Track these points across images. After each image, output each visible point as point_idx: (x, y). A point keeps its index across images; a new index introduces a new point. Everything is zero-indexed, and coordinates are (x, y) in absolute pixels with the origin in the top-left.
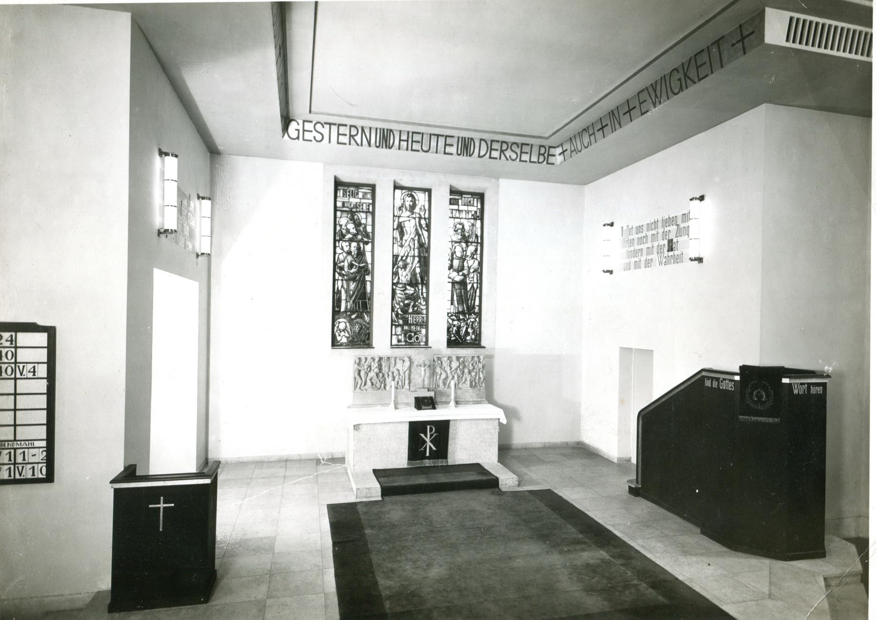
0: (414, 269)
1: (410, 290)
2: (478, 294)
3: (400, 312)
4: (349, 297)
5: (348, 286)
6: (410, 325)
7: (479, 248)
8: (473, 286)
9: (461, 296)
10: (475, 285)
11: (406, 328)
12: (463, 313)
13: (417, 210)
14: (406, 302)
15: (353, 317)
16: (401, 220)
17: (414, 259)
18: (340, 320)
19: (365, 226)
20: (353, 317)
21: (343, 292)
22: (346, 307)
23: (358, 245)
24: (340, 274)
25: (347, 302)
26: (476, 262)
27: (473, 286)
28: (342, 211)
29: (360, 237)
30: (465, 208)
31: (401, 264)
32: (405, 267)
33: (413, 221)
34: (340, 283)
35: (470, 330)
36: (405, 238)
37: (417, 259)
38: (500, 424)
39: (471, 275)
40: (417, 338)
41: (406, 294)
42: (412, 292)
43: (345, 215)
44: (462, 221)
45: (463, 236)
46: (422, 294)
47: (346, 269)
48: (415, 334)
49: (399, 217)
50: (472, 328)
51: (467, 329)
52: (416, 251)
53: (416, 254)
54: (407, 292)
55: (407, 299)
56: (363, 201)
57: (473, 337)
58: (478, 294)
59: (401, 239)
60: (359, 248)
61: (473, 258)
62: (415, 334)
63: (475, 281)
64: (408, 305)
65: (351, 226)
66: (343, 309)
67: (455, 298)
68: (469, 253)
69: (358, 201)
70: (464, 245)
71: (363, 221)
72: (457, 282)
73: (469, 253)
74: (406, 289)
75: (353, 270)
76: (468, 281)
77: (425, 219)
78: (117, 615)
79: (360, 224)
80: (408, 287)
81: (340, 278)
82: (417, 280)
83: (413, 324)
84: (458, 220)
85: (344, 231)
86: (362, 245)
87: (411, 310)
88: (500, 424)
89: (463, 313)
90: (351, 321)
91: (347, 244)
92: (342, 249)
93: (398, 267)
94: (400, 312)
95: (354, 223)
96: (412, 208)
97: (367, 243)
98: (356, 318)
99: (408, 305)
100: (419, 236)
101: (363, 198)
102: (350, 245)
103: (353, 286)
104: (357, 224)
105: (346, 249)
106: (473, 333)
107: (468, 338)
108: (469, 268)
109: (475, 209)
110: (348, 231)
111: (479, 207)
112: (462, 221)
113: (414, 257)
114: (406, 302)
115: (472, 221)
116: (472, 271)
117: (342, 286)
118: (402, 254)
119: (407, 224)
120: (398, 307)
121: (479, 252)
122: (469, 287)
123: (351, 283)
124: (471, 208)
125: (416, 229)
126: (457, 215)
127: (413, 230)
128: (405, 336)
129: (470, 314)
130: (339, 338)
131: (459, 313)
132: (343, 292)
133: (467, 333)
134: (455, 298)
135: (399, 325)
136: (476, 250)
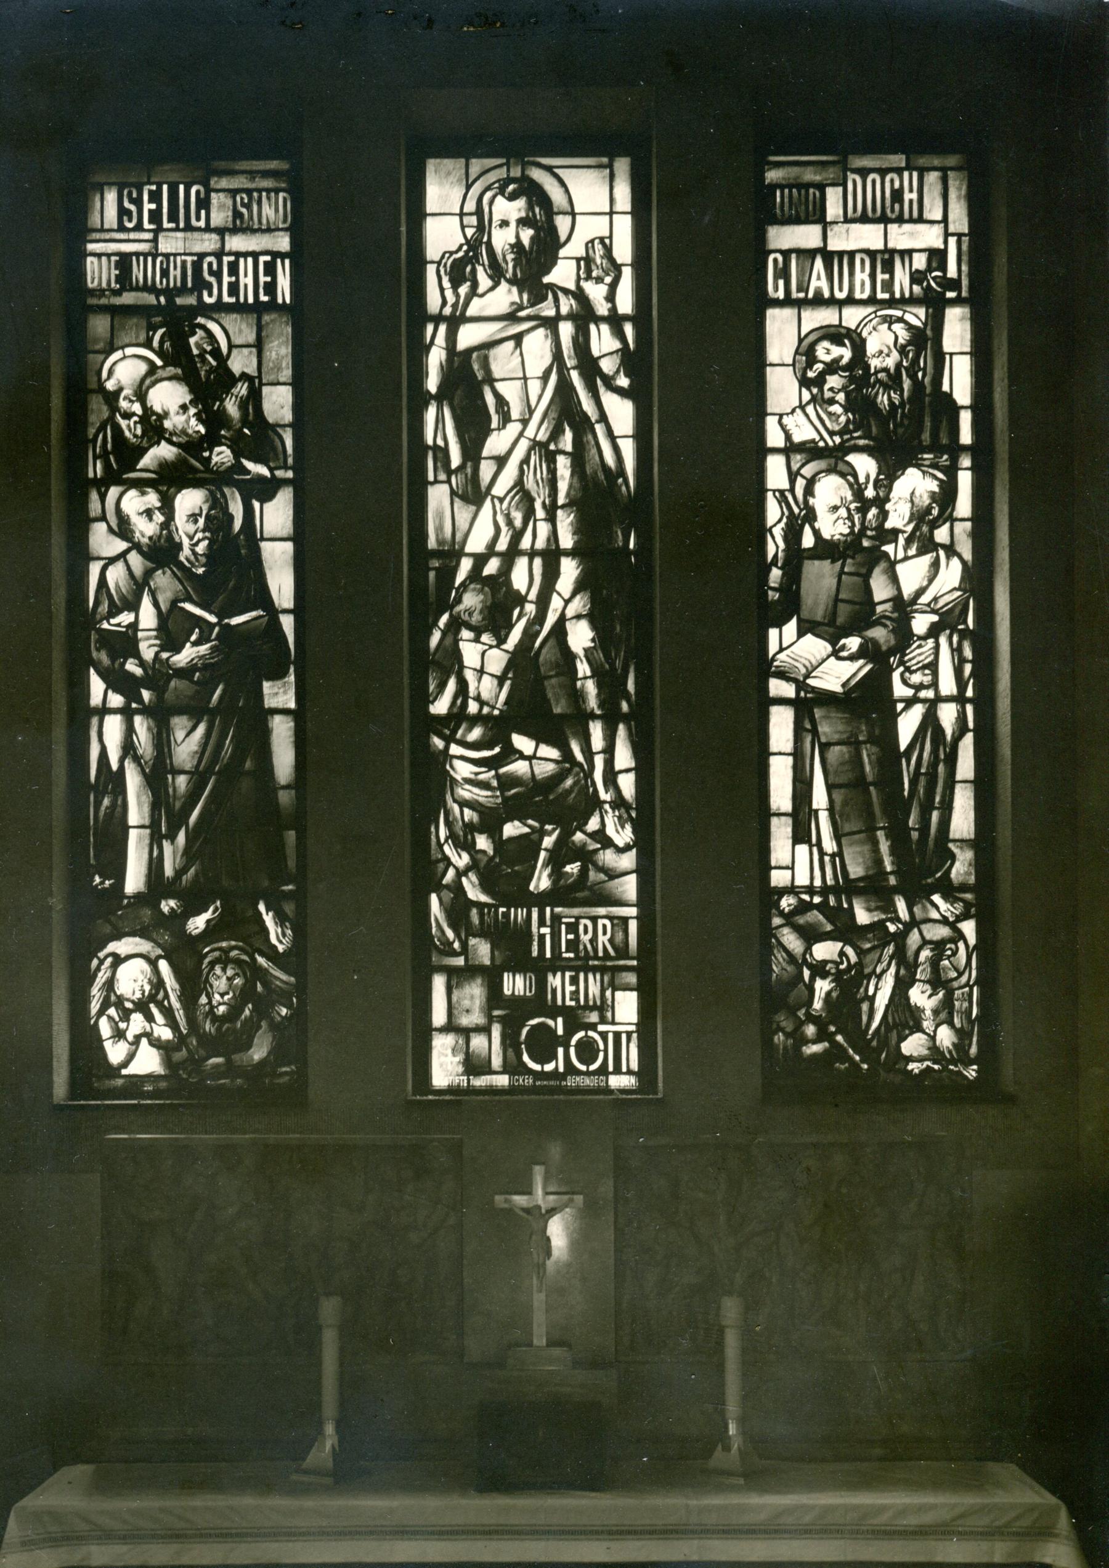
0: (560, 630)
1: (534, 757)
2: (966, 766)
3: (474, 892)
4: (165, 816)
5: (162, 740)
6: (540, 969)
7: (965, 480)
8: (930, 720)
9: (859, 783)
10: (948, 714)
11: (515, 985)
12: (874, 888)
13: (563, 274)
14: (511, 829)
15: (198, 923)
16: (469, 336)
17: (551, 574)
18: (122, 946)
19: (255, 386)
20: (198, 923)
21: (133, 780)
22: (155, 866)
23: (218, 504)
24: (117, 680)
25: (156, 838)
26: (951, 574)
27: (930, 720)
28: (115, 311)
29: (222, 455)
30: (869, 236)
31: (471, 600)
32: (496, 620)
33: (537, 345)
34: (113, 726)
35: (919, 996)
36: (496, 443)
37: (569, 570)
38: (155, 1022)
39: (920, 653)
40: (587, 1051)
41: (507, 782)
42: (543, 770)
43: (134, 329)
44: (852, 317)
45: (859, 403)
46: (611, 777)
47: (148, 652)
48: (574, 1022)
49: (456, 321)
50: (937, 982)
51: (902, 986)
52: (565, 522)
53: (567, 541)
54: (520, 767)
55: (513, 810)
56: (236, 243)
57: (945, 1037)
58: (966, 766)
59: (472, 452)
60: (216, 520)
61: (927, 545)
62: (574, 1022)
63: (948, 685)
64: (528, 846)
65: (168, 396)
66: (134, 881)
67: (820, 797)
68: (898, 516)
69: (209, 243)
70: (865, 465)
71: (241, 363)
72: (825, 698)
73: (898, 516)
74: (510, 753)
75: (186, 656)
76: (900, 690)
77: (615, 321)
78: (696, 1542)
79: (225, 379)
80: (523, 743)
81: (116, 700)
82: (577, 696)
83: (557, 964)
84: (826, 317)
85: (130, 429)
86: (236, 509)
87: (541, 881)
88: (155, 1022)
89: (874, 888)
90: (186, 955)
91: (152, 499)
92: (123, 529)
93: (456, 624)
94: (474, 892)
95: (189, 378)
96: (533, 264)
97: (266, 490)
98: (212, 931)
99: (528, 846)
100: (582, 426)
101: (239, 226)
102: (167, 507)
103: (188, 743)
104: (208, 384)
105: (146, 529)
106: (945, 1012)
107: (913, 1045)
108: (903, 608)
109: (930, 237)
110: (154, 427)
111: (959, 220)
112: (852, 317)
113: (551, 557)
114: (511, 829)
115: (917, 316)
116: (921, 624)
117: (128, 748)
118: (476, 544)
119: (502, 362)
120: (462, 860)
121: (964, 505)
122: (908, 725)
123: (179, 725)
124: (901, 237)
125: (565, 390)
126: (819, 282)
127: (543, 397)
128: (510, 1041)
129: (917, 894)
130: (115, 1053)
131: (848, 888)
132: (133, 780)
133: (905, 1020)
134: (820, 797)
135: (471, 971)
136: (947, 495)
